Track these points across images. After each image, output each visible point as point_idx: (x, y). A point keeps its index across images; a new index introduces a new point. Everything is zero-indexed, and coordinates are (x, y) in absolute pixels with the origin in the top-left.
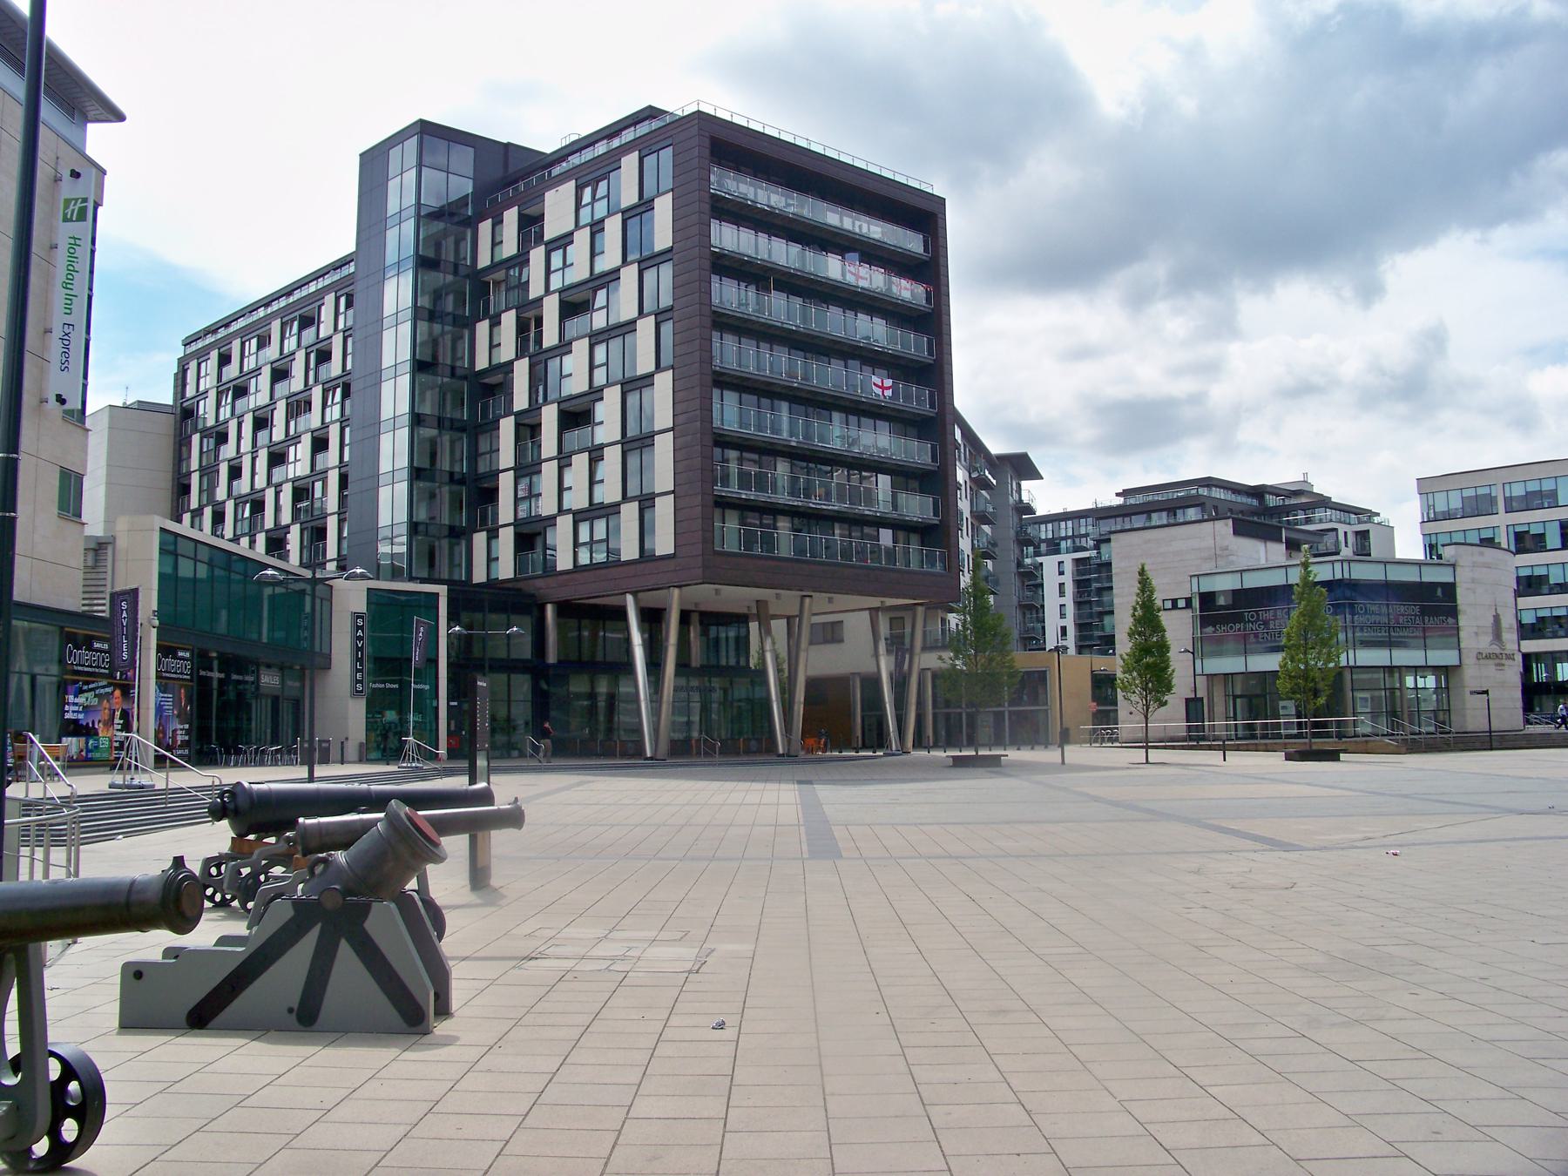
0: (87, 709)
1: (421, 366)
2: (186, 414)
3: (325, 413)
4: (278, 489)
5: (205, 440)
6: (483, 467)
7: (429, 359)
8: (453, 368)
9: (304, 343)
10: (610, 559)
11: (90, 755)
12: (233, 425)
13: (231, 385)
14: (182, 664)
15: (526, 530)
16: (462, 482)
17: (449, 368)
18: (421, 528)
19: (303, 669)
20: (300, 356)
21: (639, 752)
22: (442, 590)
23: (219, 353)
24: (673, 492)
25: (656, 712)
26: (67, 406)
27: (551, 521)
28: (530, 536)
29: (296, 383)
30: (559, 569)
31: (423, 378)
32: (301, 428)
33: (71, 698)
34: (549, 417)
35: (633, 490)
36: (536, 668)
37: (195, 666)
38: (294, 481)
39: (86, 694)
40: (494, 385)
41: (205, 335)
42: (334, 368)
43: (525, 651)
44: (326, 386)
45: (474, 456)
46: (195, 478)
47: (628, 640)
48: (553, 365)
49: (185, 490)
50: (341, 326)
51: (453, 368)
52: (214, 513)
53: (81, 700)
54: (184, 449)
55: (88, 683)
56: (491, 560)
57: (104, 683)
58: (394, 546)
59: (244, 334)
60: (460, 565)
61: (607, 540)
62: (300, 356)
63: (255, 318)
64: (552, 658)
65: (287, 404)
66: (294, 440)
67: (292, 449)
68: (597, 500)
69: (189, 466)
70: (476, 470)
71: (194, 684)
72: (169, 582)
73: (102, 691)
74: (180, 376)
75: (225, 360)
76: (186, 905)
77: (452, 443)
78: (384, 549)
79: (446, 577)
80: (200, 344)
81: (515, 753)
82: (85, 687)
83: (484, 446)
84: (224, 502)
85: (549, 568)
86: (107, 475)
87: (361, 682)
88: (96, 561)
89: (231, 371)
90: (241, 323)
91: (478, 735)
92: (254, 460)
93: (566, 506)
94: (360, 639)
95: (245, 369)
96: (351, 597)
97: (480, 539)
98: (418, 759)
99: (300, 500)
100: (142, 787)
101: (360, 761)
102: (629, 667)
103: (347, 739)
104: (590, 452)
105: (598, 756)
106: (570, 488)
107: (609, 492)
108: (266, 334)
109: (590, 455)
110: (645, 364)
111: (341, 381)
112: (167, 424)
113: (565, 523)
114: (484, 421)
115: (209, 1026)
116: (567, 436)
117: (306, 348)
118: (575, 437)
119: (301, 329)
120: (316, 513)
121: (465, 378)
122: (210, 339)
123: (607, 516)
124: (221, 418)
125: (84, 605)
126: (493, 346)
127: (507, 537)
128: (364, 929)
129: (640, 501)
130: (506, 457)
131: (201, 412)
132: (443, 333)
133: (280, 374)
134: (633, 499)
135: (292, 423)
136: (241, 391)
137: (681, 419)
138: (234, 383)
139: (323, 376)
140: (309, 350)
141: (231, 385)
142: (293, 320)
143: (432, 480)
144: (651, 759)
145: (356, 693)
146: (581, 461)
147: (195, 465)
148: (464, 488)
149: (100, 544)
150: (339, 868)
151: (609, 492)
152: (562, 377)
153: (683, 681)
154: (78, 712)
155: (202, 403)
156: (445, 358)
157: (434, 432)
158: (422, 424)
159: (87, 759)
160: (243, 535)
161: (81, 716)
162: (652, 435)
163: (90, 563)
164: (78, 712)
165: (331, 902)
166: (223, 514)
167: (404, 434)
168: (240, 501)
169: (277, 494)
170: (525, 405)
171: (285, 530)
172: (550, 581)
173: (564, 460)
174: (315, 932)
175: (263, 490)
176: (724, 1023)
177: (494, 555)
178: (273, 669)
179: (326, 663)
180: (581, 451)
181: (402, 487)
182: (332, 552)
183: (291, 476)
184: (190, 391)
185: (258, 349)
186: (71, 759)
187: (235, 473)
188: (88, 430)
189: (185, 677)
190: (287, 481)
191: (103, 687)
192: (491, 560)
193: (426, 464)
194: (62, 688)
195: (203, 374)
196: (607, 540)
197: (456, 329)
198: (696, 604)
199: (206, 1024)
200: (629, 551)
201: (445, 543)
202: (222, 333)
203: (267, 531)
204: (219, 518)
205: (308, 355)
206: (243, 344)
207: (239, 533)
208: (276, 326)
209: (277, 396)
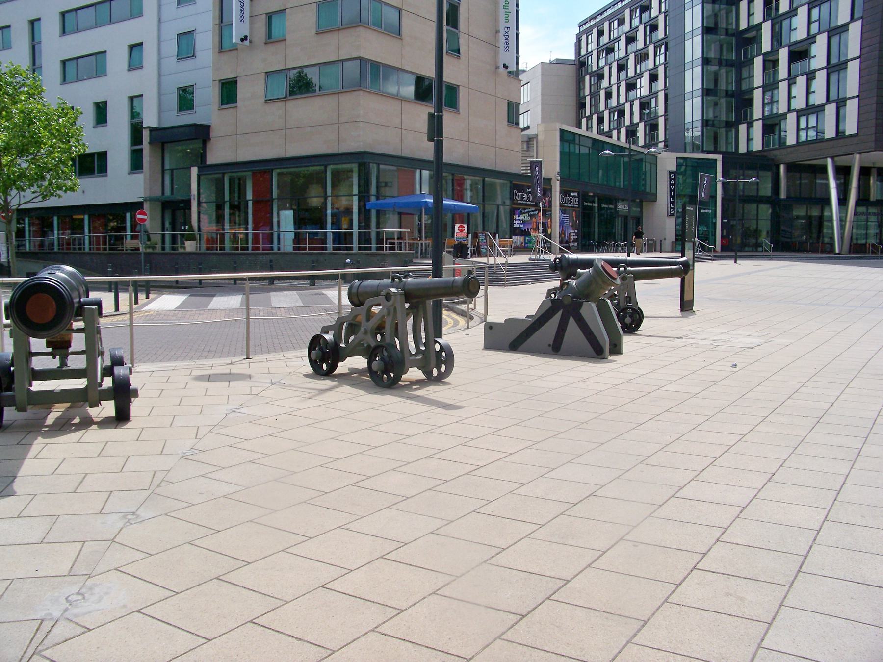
0: (524, 222)
1: (707, 31)
2: (581, 64)
3: (655, 60)
4: (632, 103)
5: (592, 78)
6: (744, 87)
7: (712, 26)
8: (727, 30)
9: (643, 21)
10: (819, 137)
11: (526, 245)
12: (606, 69)
13: (605, 47)
14: (573, 199)
15: (768, 122)
16: (732, 96)
17: (724, 30)
18: (710, 123)
19: (641, 201)
20: (641, 28)
21: (832, 250)
22: (719, 157)
23: (598, 30)
24: (858, 96)
25: (842, 227)
26: (509, 70)
27: (784, 116)
28: (772, 126)
29: (640, 44)
30: (788, 144)
31: (710, 37)
32: (643, 69)
33: (516, 217)
34: (783, 55)
35: (833, 95)
36: (773, 200)
37: (581, 200)
38: (640, 98)
39: (524, 215)
40: (749, 38)
41: (590, 20)
42: (660, 34)
43: (766, 190)
44: (656, 45)
45: (739, 80)
46: (588, 99)
47: (827, 186)
48: (786, 23)
49: (583, 106)
50: (663, 10)
51: (727, 30)
52: (598, 118)
53: (521, 217)
54: (581, 83)
55: (525, 209)
56: (749, 140)
57: (533, 209)
58: (694, 132)
59: (610, 18)
60: (732, 143)
61: (816, 127)
62: (641, 28)
63: (616, 9)
64: (783, 195)
65: (635, 56)
66: (639, 76)
67: (639, 81)
68: (811, 103)
69: (584, 93)
70: (741, 88)
71: (580, 209)
72: (566, 157)
73: (532, 213)
74: (578, 43)
75: (600, 33)
76: (471, 288)
77: (727, 73)
78: (688, 134)
79: (724, 150)
80: (588, 25)
81: (760, 249)
82: (524, 211)
83: (745, 74)
84: (603, 112)
85: (782, 142)
86: (542, 100)
87: (673, 208)
88: (528, 147)
89: (605, 39)
90: (609, 12)
91: (686, 234)
92: (618, 88)
93: (792, 108)
94: (672, 185)
95: (612, 38)
96: (668, 161)
97: (743, 128)
98: (700, 251)
99: (644, 109)
100: (545, 260)
101: (672, 251)
102: (827, 201)
103: (665, 239)
104: (807, 75)
105: (808, 251)
106: (795, 97)
107: (818, 98)
108: (622, 17)
109: (807, 76)
110: (843, 17)
111: (664, 41)
112: (571, 71)
113: (792, 118)
114: (745, 60)
115: (520, 349)
116: (794, 66)
117: (644, 24)
118: (798, 66)
119: (640, 14)
120: (652, 116)
121: (733, 35)
122: (593, 22)
123: (817, 113)
124: (601, 65)
125: (523, 170)
126: (750, 15)
127: (758, 126)
128: (580, 315)
129: (837, 103)
130: (758, 80)
131: (590, 63)
132: (720, 10)
133: (631, 40)
134: (833, 102)
135: (638, 67)
136: (610, 50)
137: (865, 50)
138: (606, 46)
139: (654, 39)
140: (646, 25)
141: (605, 47)
142: (636, 9)
143: (716, 95)
144: (839, 254)
145: (670, 215)
146: (801, 81)
147: (587, 92)
148: (734, 99)
149: (530, 138)
150: (573, 288)
151: (818, 98)
152: (791, 30)
153: (231, 211)
154: (520, 224)
155: (590, 58)
156: (723, 25)
157: (717, 68)
158: (710, 63)
159: (525, 247)
160: (614, 129)
161: (522, 226)
162: (846, 62)
163: (525, 148)
164: (520, 224)
165: (567, 301)
166: (603, 118)
167: (698, 70)
168: (611, 111)
169: (631, 106)
170: (769, 49)
171: (636, 126)
172: (784, 151)
173: (791, 80)
174: (560, 313)
175: (624, 104)
176: (736, 365)
177: (751, 137)
178: (625, 202)
179: (653, 198)
180: (801, 75)
181: (698, 100)
182: (661, 137)
183: (638, 95)
184: (583, 52)
185: (618, 26)
186: (517, 247)
187: (609, 95)
188: (521, 81)
189: (575, 206)
190: (637, 98)
191: (533, 211)
192: (749, 140)
193: (712, 87)
194: (512, 212)
195: (589, 42)
196: (816, 127)
197: (728, 7)
198: (873, 163)
199: (517, 348)
200: (830, 132)
201: (722, 132)
202: (599, 18)
203: (627, 127)
204: (601, 120)
205: (645, 28)
206: (610, 24)
207: (612, 128)
208: (627, 12)
209: (630, 51)
